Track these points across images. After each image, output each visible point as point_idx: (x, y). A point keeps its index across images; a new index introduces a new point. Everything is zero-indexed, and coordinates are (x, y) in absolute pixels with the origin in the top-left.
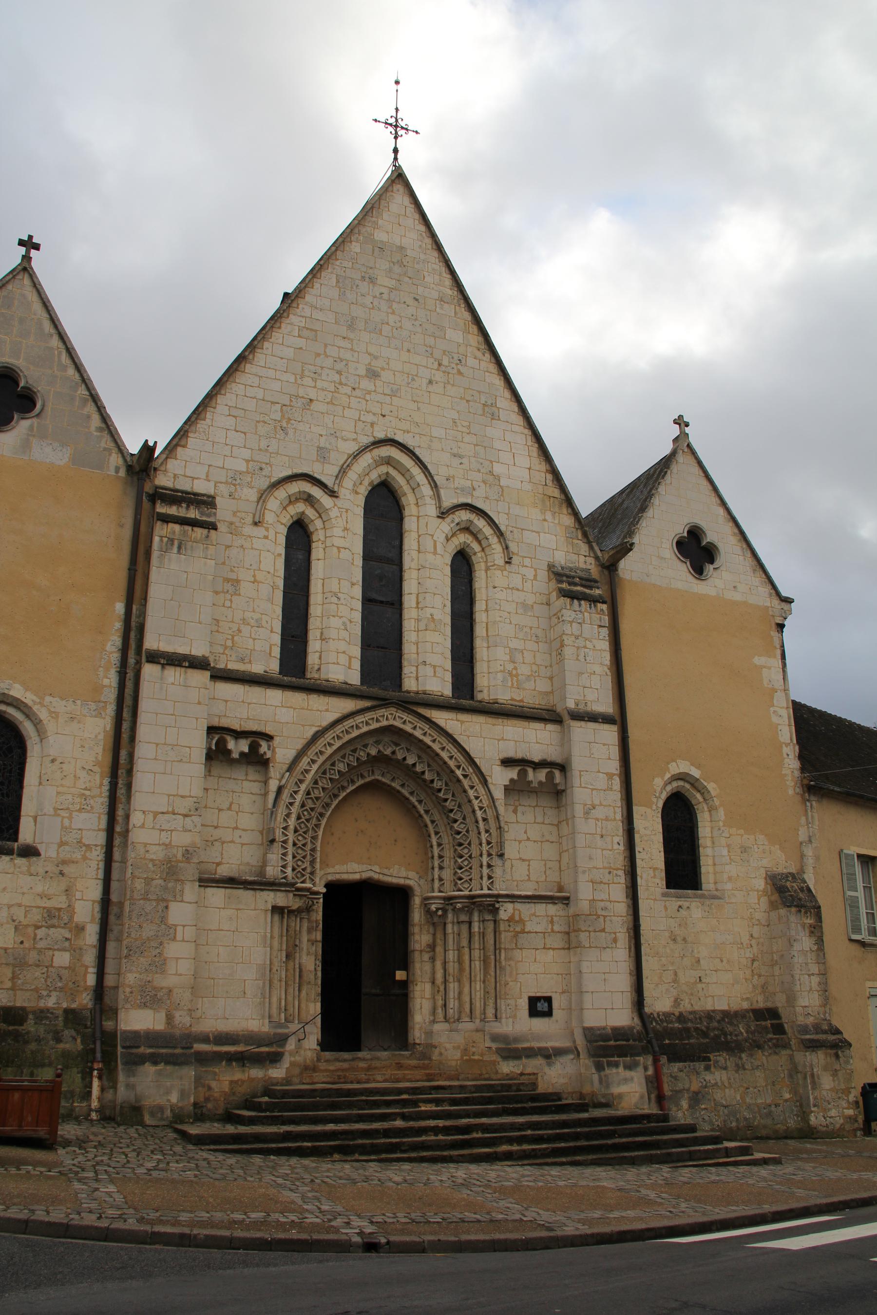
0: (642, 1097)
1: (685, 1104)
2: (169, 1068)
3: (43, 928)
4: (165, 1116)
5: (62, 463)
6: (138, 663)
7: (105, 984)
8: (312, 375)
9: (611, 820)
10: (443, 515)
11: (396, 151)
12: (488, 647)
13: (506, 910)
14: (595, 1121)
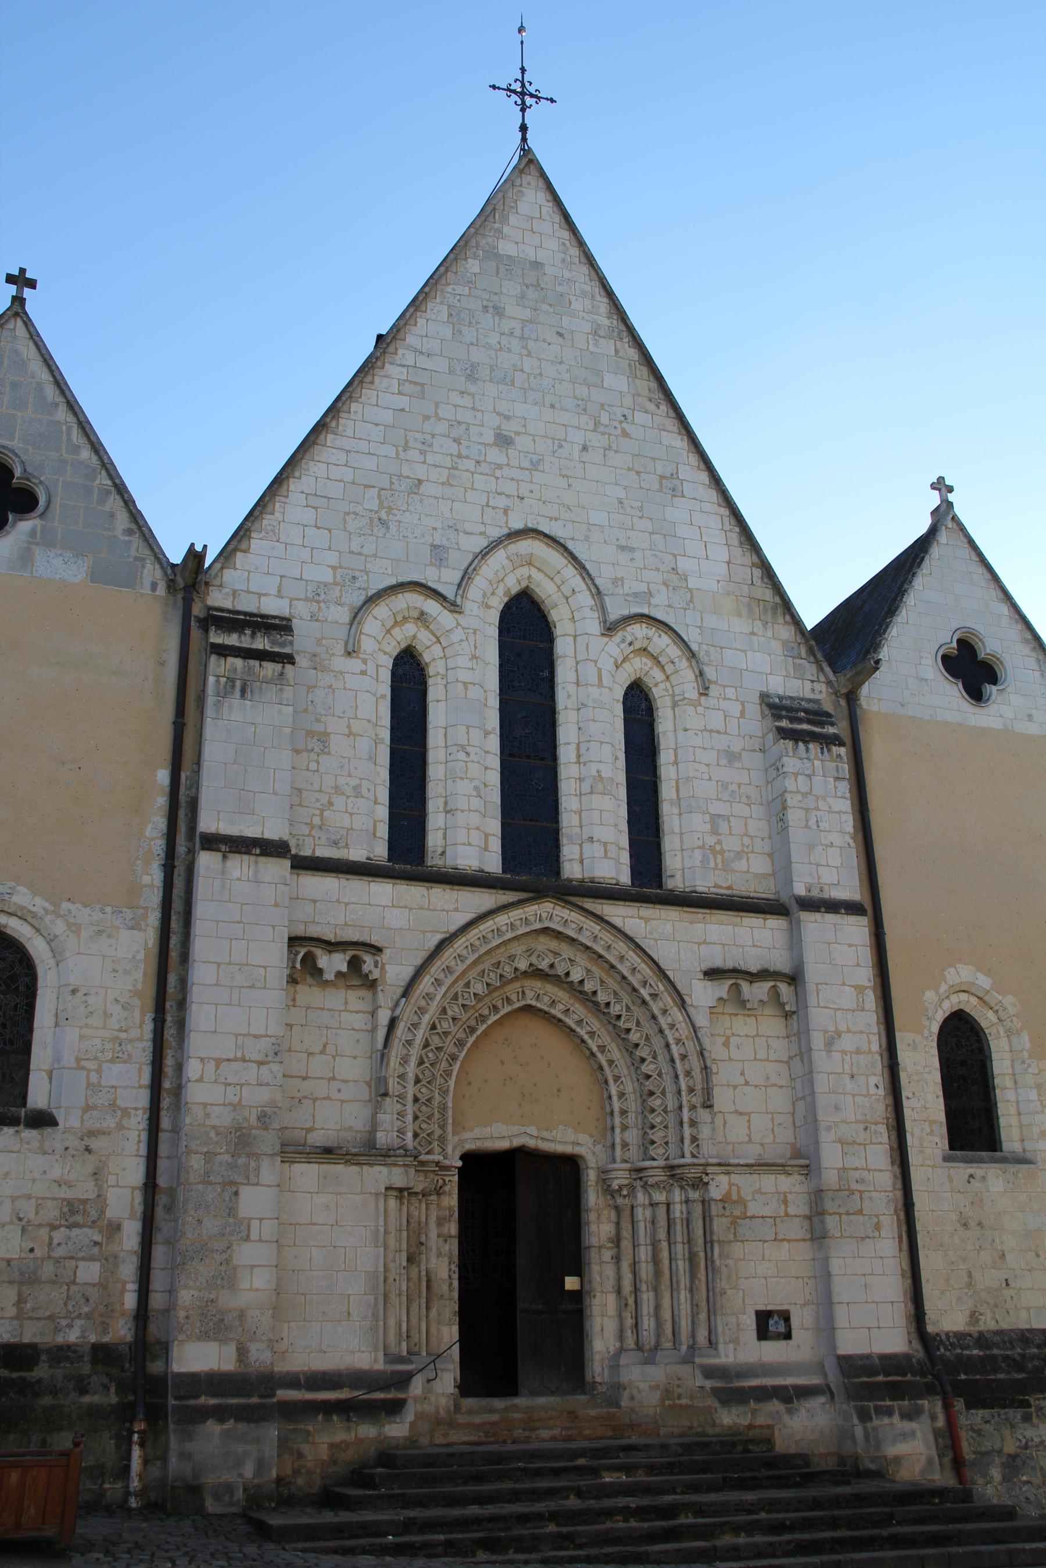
0: (930, 1461)
1: (996, 1473)
2: (242, 1426)
3: (62, 1229)
4: (235, 1499)
5: (76, 580)
6: (191, 852)
7: (150, 1307)
8: (420, 446)
9: (865, 1052)
10: (610, 628)
11: (524, 128)
12: (680, 814)
13: (719, 1186)
14: (860, 1499)
